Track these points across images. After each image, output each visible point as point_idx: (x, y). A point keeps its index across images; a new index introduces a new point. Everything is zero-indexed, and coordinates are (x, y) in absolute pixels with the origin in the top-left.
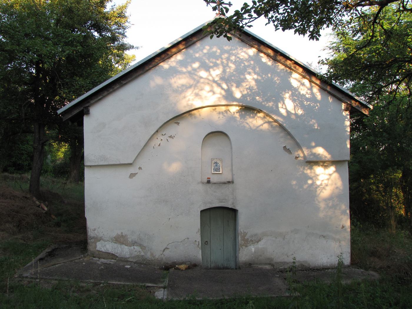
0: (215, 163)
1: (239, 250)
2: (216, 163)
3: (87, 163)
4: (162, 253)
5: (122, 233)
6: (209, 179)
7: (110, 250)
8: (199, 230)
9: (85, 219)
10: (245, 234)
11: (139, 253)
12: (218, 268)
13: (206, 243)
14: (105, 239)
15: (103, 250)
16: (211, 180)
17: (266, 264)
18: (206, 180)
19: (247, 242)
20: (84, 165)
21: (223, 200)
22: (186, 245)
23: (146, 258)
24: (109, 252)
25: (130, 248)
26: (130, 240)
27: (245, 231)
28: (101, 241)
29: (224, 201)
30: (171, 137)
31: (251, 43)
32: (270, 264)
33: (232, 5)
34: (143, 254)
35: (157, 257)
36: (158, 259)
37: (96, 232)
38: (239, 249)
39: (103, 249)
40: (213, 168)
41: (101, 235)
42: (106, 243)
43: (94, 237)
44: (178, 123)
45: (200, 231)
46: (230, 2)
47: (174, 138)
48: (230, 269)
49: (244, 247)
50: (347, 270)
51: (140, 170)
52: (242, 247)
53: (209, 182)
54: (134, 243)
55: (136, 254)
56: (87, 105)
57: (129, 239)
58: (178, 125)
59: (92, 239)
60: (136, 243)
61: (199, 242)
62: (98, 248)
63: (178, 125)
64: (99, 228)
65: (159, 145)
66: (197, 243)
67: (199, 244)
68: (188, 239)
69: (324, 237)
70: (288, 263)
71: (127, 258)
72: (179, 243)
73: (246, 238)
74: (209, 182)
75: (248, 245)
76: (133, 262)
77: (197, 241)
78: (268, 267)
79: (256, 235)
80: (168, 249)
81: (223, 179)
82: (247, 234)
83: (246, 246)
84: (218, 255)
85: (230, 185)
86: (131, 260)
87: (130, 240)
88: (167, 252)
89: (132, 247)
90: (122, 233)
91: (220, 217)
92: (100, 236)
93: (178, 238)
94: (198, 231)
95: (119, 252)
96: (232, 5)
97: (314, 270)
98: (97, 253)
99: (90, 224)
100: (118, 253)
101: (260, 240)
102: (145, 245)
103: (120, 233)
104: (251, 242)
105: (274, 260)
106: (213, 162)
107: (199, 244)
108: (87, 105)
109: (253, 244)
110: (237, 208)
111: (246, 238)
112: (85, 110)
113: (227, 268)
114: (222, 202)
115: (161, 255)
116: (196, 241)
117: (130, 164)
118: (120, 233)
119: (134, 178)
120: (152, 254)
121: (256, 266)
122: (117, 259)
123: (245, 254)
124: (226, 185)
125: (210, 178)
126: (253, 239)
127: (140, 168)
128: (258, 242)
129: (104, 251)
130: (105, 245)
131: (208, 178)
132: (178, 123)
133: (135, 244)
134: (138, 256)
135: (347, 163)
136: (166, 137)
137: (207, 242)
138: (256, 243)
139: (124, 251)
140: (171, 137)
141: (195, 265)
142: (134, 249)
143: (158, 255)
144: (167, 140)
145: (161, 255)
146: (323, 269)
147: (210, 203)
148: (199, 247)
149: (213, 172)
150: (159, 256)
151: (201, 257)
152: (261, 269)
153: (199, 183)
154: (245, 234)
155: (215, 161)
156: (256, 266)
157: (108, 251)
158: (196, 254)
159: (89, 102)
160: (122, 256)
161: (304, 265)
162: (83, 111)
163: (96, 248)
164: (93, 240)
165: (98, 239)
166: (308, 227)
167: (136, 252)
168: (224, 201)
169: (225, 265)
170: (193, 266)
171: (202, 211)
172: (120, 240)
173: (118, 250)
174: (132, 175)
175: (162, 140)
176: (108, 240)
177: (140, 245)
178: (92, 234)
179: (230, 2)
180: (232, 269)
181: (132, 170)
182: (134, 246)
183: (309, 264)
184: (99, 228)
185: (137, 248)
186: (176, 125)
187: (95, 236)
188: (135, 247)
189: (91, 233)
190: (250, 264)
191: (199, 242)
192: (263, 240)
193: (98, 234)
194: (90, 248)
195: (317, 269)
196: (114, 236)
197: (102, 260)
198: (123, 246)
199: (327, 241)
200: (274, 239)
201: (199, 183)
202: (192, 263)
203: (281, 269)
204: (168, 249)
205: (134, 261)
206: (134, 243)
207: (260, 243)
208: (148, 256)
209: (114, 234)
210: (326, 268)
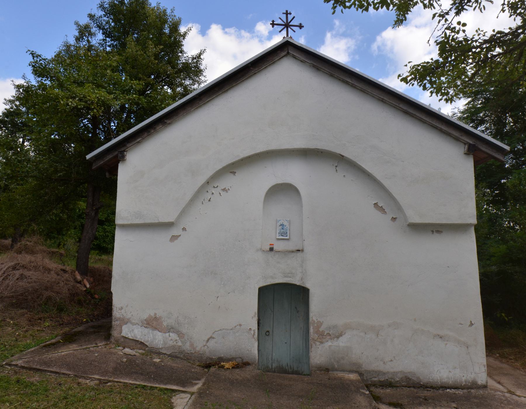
0: (281, 225)
1: (312, 347)
2: (282, 225)
3: (118, 221)
4: (205, 344)
5: (155, 314)
6: (272, 246)
7: (139, 337)
8: (255, 314)
9: (112, 293)
10: (320, 324)
11: (175, 343)
12: (282, 370)
13: (267, 334)
14: (134, 321)
15: (130, 336)
16: (275, 248)
17: (351, 372)
18: (268, 248)
19: (322, 336)
20: (115, 225)
21: (289, 273)
22: (237, 334)
23: (184, 351)
24: (137, 339)
25: (164, 335)
26: (165, 324)
27: (319, 320)
28: (129, 324)
29: (290, 275)
30: (224, 190)
31: (33, 275)
32: (356, 372)
33: (303, 27)
34: (180, 344)
35: (198, 349)
36: (199, 351)
37: (123, 311)
38: (311, 346)
39: (129, 335)
40: (278, 232)
41: (129, 316)
42: (134, 326)
43: (120, 318)
44: (234, 173)
45: (257, 316)
46: (301, 24)
47: (229, 191)
48: (301, 375)
49: (318, 343)
50: (481, 392)
51: (184, 232)
52: (314, 343)
53: (271, 249)
54: (170, 329)
55: (171, 343)
56: (123, 149)
57: (163, 323)
58: (234, 175)
59: (117, 321)
60: (173, 328)
61: (254, 331)
62: (124, 334)
63: (234, 175)
64: (127, 306)
65: (209, 200)
66: (252, 332)
67: (254, 334)
68: (240, 325)
69: (441, 337)
70: (384, 374)
71: (159, 349)
72: (229, 331)
73: (321, 330)
74: (271, 249)
75: (324, 340)
76: (167, 355)
77: (253, 329)
78: (353, 377)
79: (335, 327)
80: (213, 338)
81: (291, 246)
82: (322, 324)
83: (322, 343)
84: (282, 352)
85: (299, 254)
86: (164, 352)
87: (165, 324)
88: (211, 344)
89: (167, 334)
90: (155, 314)
91: (283, 300)
92: (127, 317)
93: (229, 324)
94: (255, 316)
95: (150, 339)
96: (303, 27)
97: (427, 387)
98: (122, 340)
99: (117, 301)
100: (148, 341)
101: (341, 335)
102: (184, 331)
103: (153, 315)
104: (328, 337)
105: (363, 366)
106: (279, 224)
107: (254, 334)
108: (123, 149)
109: (331, 339)
110: (308, 285)
111: (321, 330)
112: (120, 155)
113: (297, 373)
114: (285, 277)
115: (204, 346)
116: (250, 329)
117: (169, 225)
118: (153, 315)
119: (176, 241)
120: (192, 345)
121: (340, 374)
122: (147, 349)
123: (319, 355)
124: (293, 254)
125: (273, 245)
126: (330, 333)
127: (184, 229)
128: (338, 337)
129: (131, 338)
130: (133, 330)
131: (270, 244)
132: (234, 173)
133: (172, 330)
134: (173, 347)
135: (472, 230)
136: (219, 189)
137: (268, 332)
138: (336, 339)
139: (157, 339)
140: (224, 190)
141: (247, 364)
142: (170, 336)
143: (199, 346)
144: (220, 193)
145: (204, 346)
146: (442, 387)
147: (272, 277)
148: (254, 338)
149: (278, 237)
150: (201, 348)
151: (256, 352)
152: (340, 379)
153: (257, 250)
154: (320, 324)
155: (281, 222)
156: (335, 373)
157: (137, 338)
158: (250, 347)
159: (125, 146)
160: (153, 346)
161: (410, 379)
162: (117, 156)
163: (121, 333)
164: (118, 322)
165: (125, 321)
166: (415, 320)
167: (172, 341)
168: (290, 275)
169: (295, 369)
170: (242, 364)
171: (262, 291)
172: (152, 323)
173: (148, 337)
174: (174, 238)
175: (213, 193)
176: (137, 323)
177: (180, 335)
178: (117, 313)
179: (301, 24)
180: (304, 375)
181: (175, 231)
182: (169, 332)
183: (418, 378)
184: (127, 306)
185: (174, 336)
186: (232, 175)
187: (121, 317)
188: (171, 334)
189: (116, 313)
190: (327, 369)
191: (254, 331)
192: (346, 334)
193: (125, 315)
194: (115, 333)
195: (432, 387)
196: (146, 318)
197: (127, 350)
198: (156, 332)
199: (446, 344)
200: (362, 334)
201: (257, 250)
202: (244, 361)
203: (375, 381)
204: (213, 338)
205: (168, 353)
206: (170, 329)
207: (340, 338)
208: (187, 347)
209: (146, 316)
210: (447, 386)
